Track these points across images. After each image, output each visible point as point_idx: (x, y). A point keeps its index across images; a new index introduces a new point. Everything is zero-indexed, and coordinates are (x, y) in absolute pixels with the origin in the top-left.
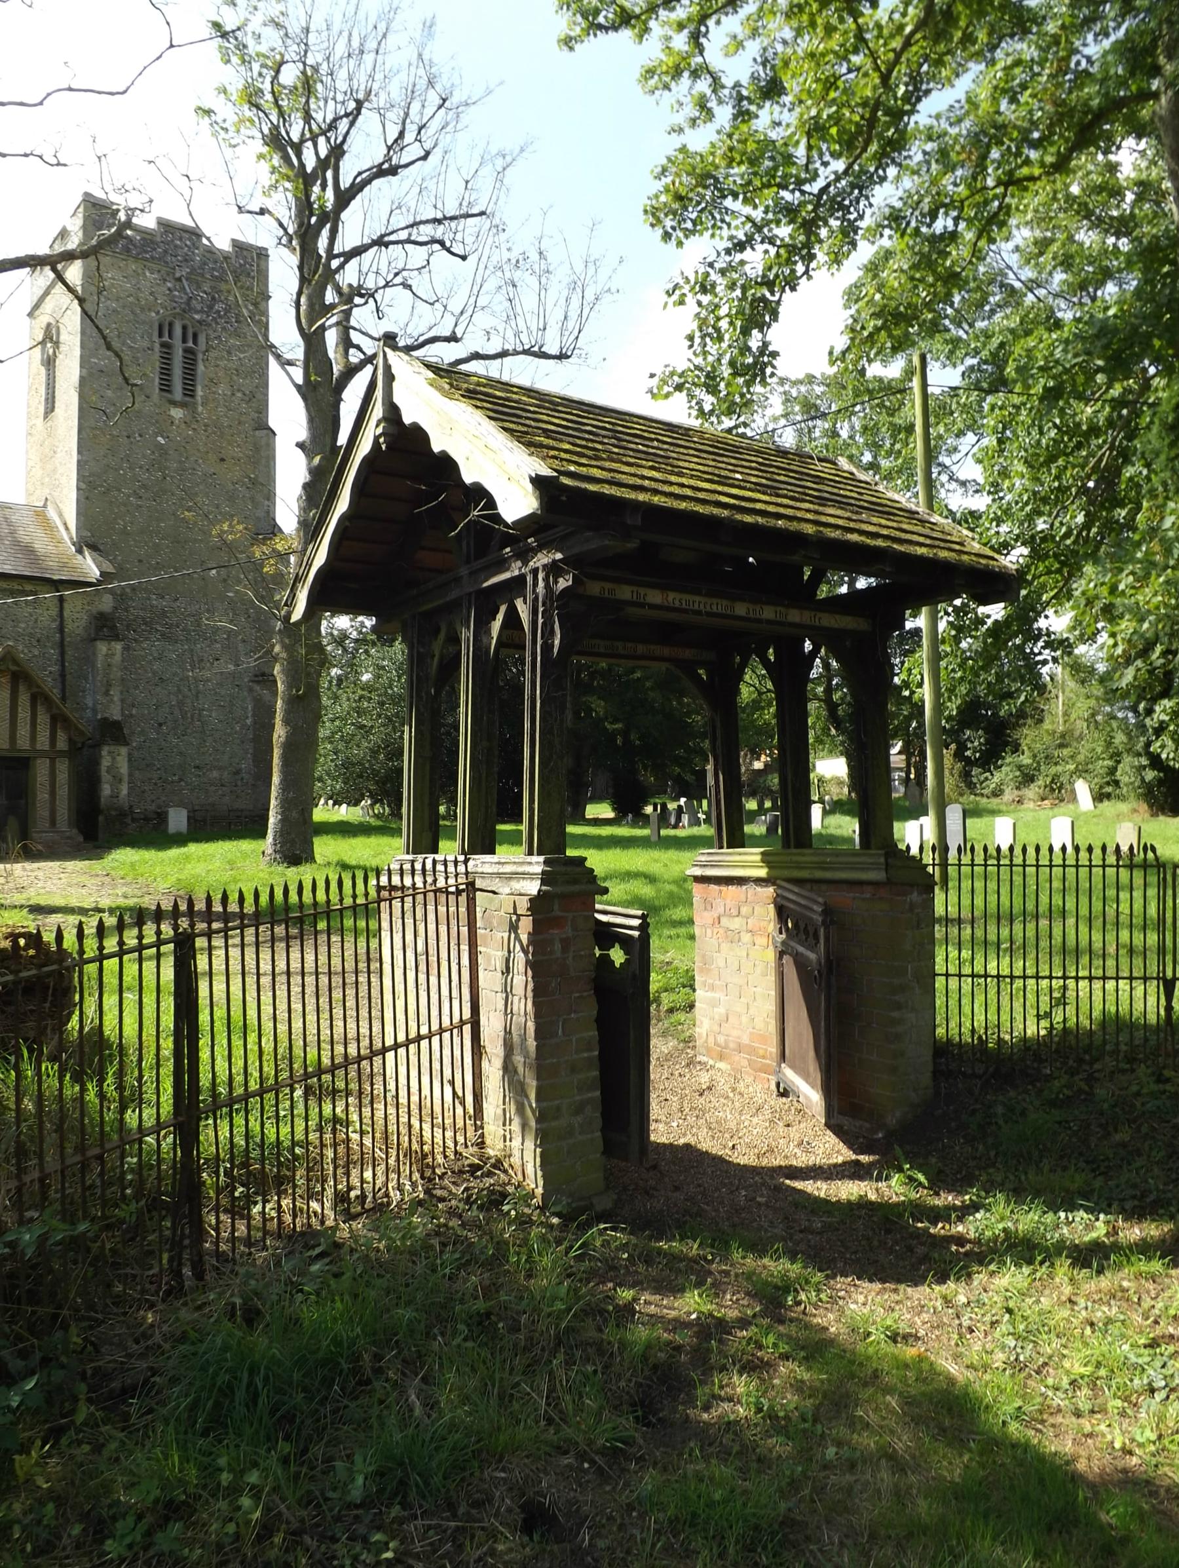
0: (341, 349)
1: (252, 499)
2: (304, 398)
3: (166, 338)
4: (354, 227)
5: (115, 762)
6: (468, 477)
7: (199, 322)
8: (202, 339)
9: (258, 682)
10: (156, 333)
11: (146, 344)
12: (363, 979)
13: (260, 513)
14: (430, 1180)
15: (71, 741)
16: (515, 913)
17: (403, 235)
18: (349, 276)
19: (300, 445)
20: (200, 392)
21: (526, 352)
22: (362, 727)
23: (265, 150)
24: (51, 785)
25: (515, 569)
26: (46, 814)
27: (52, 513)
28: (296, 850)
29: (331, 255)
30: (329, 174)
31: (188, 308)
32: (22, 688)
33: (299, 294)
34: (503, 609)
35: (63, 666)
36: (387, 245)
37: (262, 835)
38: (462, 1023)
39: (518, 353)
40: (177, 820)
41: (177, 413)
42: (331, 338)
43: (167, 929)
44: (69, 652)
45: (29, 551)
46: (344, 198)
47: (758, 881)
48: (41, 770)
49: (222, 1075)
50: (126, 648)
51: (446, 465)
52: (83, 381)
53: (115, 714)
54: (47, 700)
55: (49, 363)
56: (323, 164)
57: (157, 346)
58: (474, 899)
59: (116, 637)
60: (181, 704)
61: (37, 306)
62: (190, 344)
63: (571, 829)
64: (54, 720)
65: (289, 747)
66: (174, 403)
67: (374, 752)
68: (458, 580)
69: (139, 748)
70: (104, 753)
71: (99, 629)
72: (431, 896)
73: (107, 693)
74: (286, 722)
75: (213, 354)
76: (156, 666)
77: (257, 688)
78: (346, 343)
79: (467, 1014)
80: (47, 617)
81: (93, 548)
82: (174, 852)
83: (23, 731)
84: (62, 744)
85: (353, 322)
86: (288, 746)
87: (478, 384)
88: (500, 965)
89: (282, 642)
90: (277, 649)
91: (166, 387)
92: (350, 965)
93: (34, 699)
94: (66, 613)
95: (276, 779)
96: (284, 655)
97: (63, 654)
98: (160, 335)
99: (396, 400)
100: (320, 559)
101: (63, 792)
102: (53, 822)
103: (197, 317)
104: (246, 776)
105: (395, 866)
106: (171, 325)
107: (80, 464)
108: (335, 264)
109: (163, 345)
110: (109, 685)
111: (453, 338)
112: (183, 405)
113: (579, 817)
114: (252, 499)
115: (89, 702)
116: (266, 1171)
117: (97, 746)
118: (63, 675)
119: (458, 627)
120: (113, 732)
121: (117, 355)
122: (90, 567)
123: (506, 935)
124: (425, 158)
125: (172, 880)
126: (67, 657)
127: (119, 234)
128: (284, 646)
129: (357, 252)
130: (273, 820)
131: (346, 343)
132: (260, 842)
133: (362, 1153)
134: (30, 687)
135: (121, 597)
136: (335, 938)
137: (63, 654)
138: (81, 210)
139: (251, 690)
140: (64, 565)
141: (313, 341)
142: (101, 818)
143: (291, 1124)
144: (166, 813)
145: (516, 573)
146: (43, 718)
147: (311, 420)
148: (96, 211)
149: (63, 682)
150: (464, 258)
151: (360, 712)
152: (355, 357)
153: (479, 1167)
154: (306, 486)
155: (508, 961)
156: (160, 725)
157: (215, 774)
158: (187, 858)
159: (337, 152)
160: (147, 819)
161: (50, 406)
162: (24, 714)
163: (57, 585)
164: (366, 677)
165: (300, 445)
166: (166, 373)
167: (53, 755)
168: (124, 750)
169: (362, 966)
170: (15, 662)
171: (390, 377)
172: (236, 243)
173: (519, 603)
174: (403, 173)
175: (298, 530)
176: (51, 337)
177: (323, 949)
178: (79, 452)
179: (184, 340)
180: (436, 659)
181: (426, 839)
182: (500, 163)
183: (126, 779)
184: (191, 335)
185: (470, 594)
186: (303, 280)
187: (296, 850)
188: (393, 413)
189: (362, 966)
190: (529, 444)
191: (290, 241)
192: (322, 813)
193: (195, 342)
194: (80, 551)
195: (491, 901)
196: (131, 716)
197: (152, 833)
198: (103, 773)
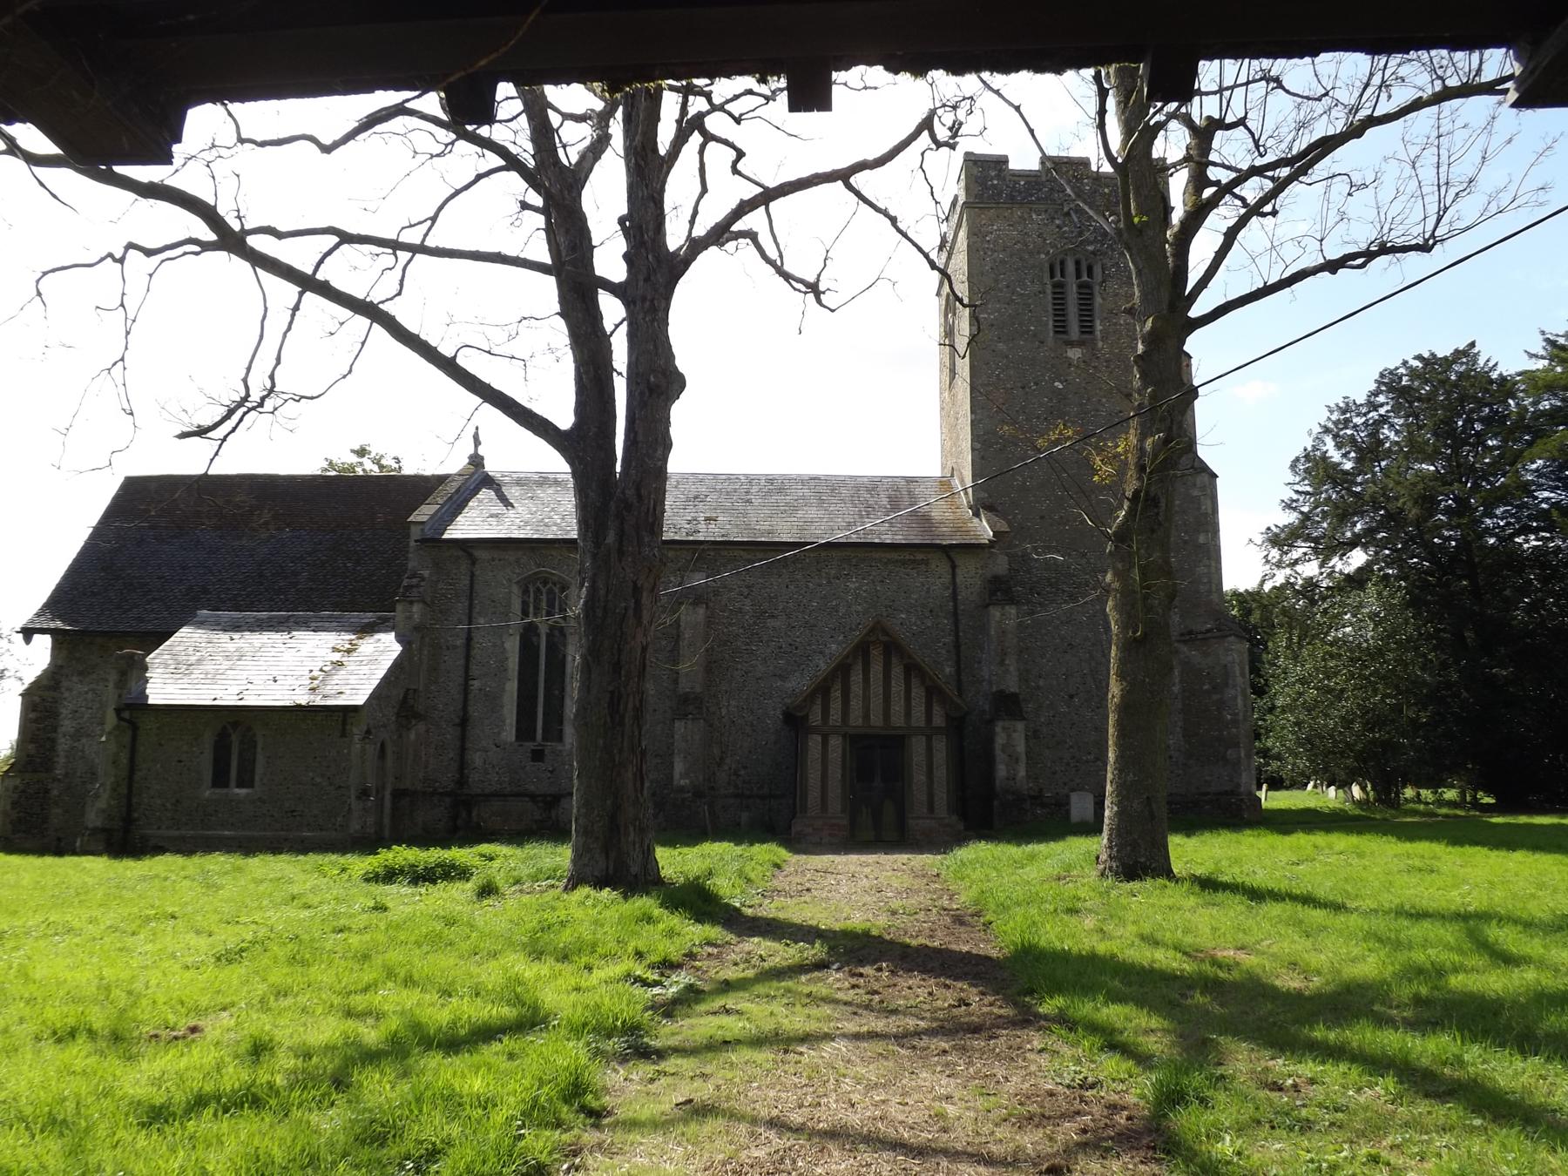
3: (1058, 278)
5: (1011, 738)
7: (1093, 253)
8: (1097, 270)
9: (1185, 642)
10: (1047, 275)
11: (1037, 288)
15: (948, 717)
22: (1330, 691)
24: (929, 769)
32: (894, 660)
35: (957, 636)
41: (1075, 354)
45: (924, 520)
47: (1215, 164)
48: (918, 746)
53: (1012, 685)
57: (1049, 289)
59: (1012, 601)
62: (1085, 278)
66: (1071, 344)
67: (1347, 722)
70: (998, 729)
71: (992, 593)
73: (1002, 663)
74: (1121, 676)
81: (990, 508)
83: (898, 707)
84: (939, 720)
86: (1125, 708)
91: (1061, 328)
94: (959, 580)
96: (1116, 585)
97: (956, 623)
98: (1052, 276)
101: (941, 773)
102: (931, 809)
103: (1090, 248)
106: (1062, 263)
107: (974, 424)
109: (1056, 285)
112: (1080, 344)
117: (991, 722)
118: (957, 646)
120: (1008, 705)
122: (984, 529)
126: (961, 627)
132: (1096, 839)
137: (956, 623)
140: (958, 530)
142: (996, 803)
146: (918, 693)
156: (1071, 697)
162: (897, 687)
163: (949, 552)
164: (1109, 577)
168: (1020, 726)
170: (885, 632)
179: (1078, 276)
193: (1090, 274)
194: (977, 514)
196: (1038, 688)
198: (998, 752)
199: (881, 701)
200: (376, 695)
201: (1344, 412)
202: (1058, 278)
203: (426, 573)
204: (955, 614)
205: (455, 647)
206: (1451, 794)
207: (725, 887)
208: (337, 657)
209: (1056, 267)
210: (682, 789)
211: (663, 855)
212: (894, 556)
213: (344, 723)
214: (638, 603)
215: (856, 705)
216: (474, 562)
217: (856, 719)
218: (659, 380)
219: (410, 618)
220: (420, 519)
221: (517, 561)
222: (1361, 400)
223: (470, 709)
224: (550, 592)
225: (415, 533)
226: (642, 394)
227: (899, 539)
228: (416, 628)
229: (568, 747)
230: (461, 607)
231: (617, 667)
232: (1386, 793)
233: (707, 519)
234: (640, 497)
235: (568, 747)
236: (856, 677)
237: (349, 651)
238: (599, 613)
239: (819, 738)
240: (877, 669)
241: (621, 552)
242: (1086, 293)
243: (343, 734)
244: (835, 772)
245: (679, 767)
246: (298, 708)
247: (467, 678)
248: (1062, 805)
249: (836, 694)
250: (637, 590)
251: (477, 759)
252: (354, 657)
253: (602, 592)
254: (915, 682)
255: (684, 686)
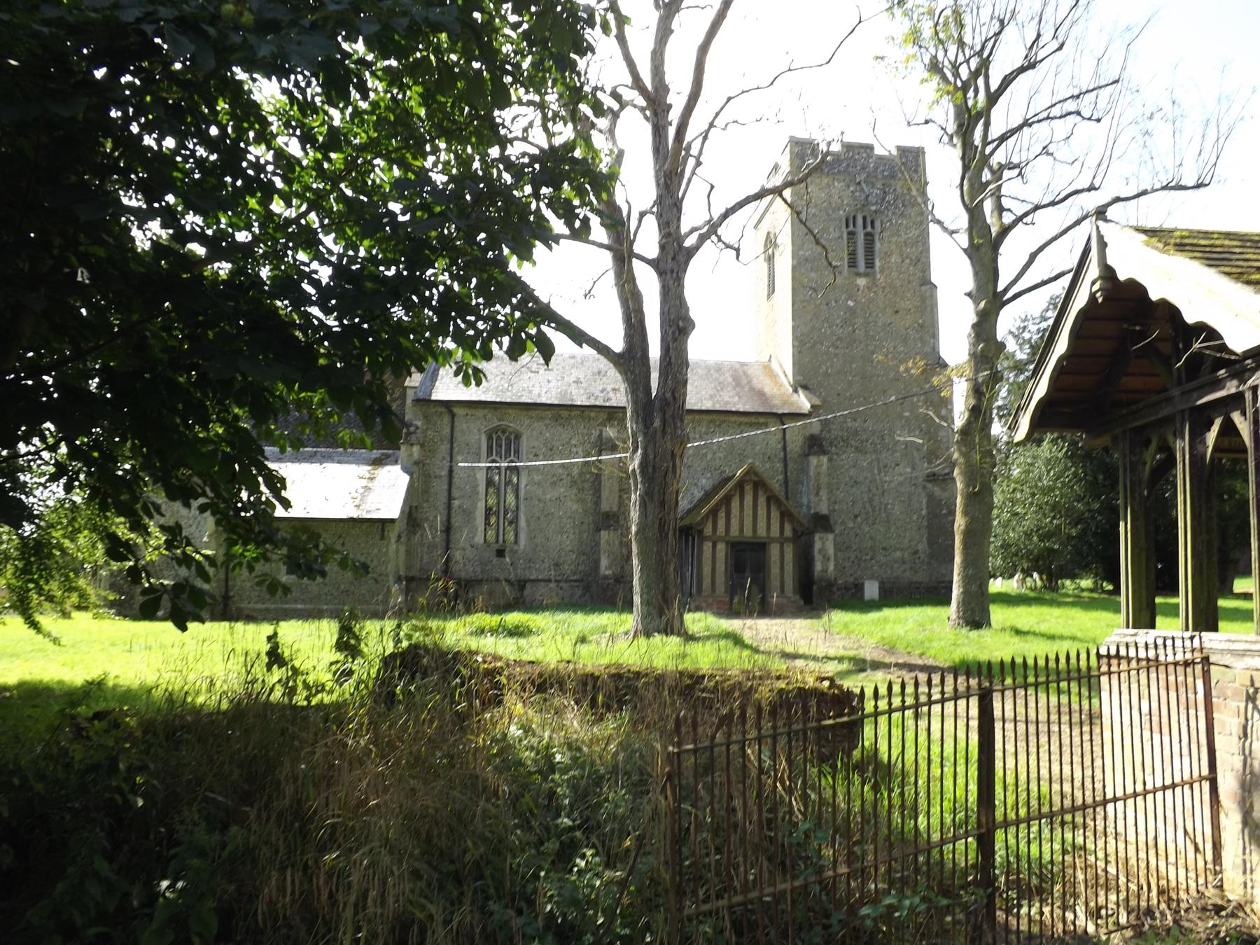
0: (996, 214)
1: (921, 339)
2: (970, 257)
4: (1001, 119)
5: (824, 544)
6: (1190, 318)
7: (876, 212)
8: (877, 224)
11: (837, 235)
12: (1055, 728)
13: (927, 349)
14: (1177, 912)
15: (794, 530)
16: (1252, 685)
17: (1045, 114)
18: (999, 157)
19: (969, 295)
20: (878, 263)
21: (1164, 188)
23: (926, 75)
24: (781, 563)
25: (1231, 388)
26: (778, 584)
27: (775, 366)
28: (975, 618)
29: (985, 143)
30: (981, 81)
31: (866, 203)
32: (760, 493)
33: (963, 178)
34: (1218, 422)
35: (786, 476)
36: (1030, 125)
37: (946, 601)
38: (1201, 778)
39: (1154, 191)
40: (871, 590)
41: (862, 282)
42: (988, 206)
43: (973, 682)
44: (791, 465)
45: (761, 394)
46: (993, 98)
48: (774, 550)
49: (1011, 800)
50: (830, 460)
51: (1169, 312)
52: (794, 268)
53: (824, 509)
54: (779, 503)
55: (770, 260)
56: (975, 75)
57: (845, 235)
58: (1209, 671)
59: (824, 453)
60: (871, 500)
61: (759, 221)
63: (1222, 603)
64: (783, 515)
65: (968, 534)
66: (859, 275)
67: (1028, 535)
68: (1169, 400)
69: (841, 534)
71: (811, 447)
72: (1171, 668)
73: (817, 494)
74: (965, 513)
75: (886, 234)
76: (852, 472)
77: (929, 485)
78: (1000, 209)
79: (1205, 772)
80: (775, 443)
81: (805, 387)
82: (874, 615)
83: (762, 524)
84: (788, 532)
85: (1003, 193)
87: (1182, 237)
88: (1236, 729)
89: (959, 450)
90: (956, 456)
91: (853, 263)
92: (1043, 717)
93: (769, 500)
95: (958, 559)
96: (962, 460)
97: (786, 466)
98: (847, 226)
99: (1109, 262)
100: (1042, 389)
101: (789, 568)
104: (923, 556)
105: (1151, 642)
106: (854, 218)
108: (988, 150)
109: (850, 233)
110: (818, 488)
111: (1092, 188)
112: (866, 275)
113: (1229, 593)
114: (921, 339)
115: (805, 501)
116: (1038, 882)
117: (811, 533)
118: (786, 481)
119: (1170, 439)
120: (822, 522)
121: (824, 247)
123: (1242, 705)
124: (1061, 47)
125: (877, 637)
126: (789, 468)
127: (823, 160)
128: (961, 453)
129: (1003, 138)
130: (956, 591)
131: (1000, 209)
133: (1107, 879)
134: (766, 492)
135: (825, 423)
136: (1020, 692)
137: (786, 466)
138: (788, 149)
139: (924, 488)
140: (785, 403)
141: (975, 213)
142: (815, 588)
143: (1045, 846)
144: (863, 584)
145: (1233, 391)
146: (775, 514)
147: (976, 274)
148: (801, 149)
149: (787, 487)
150: (1098, 120)
151: (1014, 502)
152: (1008, 218)
153: (1223, 908)
154: (975, 326)
155: (1245, 728)
157: (898, 554)
158: (886, 620)
159: (985, 65)
160: (847, 589)
161: (771, 290)
162: (762, 511)
163: (782, 418)
165: (969, 295)
166: (853, 255)
167: (782, 541)
168: (831, 537)
169: (1054, 717)
170: (756, 474)
171: (1103, 245)
172: (899, 148)
173: (1236, 417)
174: (1039, 66)
175: (969, 361)
176: (771, 241)
177: (1021, 702)
178: (793, 320)
179: (865, 227)
180: (1148, 467)
181: (1145, 617)
182: (1128, 37)
183: (832, 558)
184: (869, 222)
185: (1183, 411)
186: (966, 168)
187: (975, 618)
188: (1108, 273)
189: (1054, 717)
190: (1248, 283)
191: (951, 137)
192: (997, 586)
193: (873, 226)
195: (1224, 674)
197: (853, 599)
199: (750, 519)
200: (402, 512)
201: (1024, 321)
202: (851, 228)
203: (419, 423)
204: (785, 460)
205: (440, 477)
206: (1086, 583)
207: (747, 637)
208: (365, 482)
209: (850, 221)
210: (606, 577)
211: (688, 617)
212: (745, 419)
213: (383, 530)
214: (674, 464)
215: (735, 522)
216: (453, 415)
217: (734, 531)
218: (678, 324)
219: (411, 455)
220: (413, 384)
221: (485, 416)
222: (1037, 314)
223: (453, 521)
224: (508, 439)
225: (410, 395)
226: (674, 333)
227: (748, 408)
228: (416, 463)
229: (522, 548)
230: (445, 447)
231: (662, 503)
232: (1052, 584)
233: (614, 390)
234: (674, 398)
235: (522, 548)
236: (735, 504)
237: (371, 479)
238: (650, 470)
239: (710, 544)
240: (749, 499)
241: (664, 432)
242: (870, 238)
243: (382, 538)
244: (721, 567)
245: (604, 562)
246: (352, 520)
247: (450, 498)
248: (859, 588)
249: (722, 514)
250: (673, 455)
251: (458, 555)
252: (376, 482)
253: (651, 457)
254: (773, 508)
255: (605, 506)
